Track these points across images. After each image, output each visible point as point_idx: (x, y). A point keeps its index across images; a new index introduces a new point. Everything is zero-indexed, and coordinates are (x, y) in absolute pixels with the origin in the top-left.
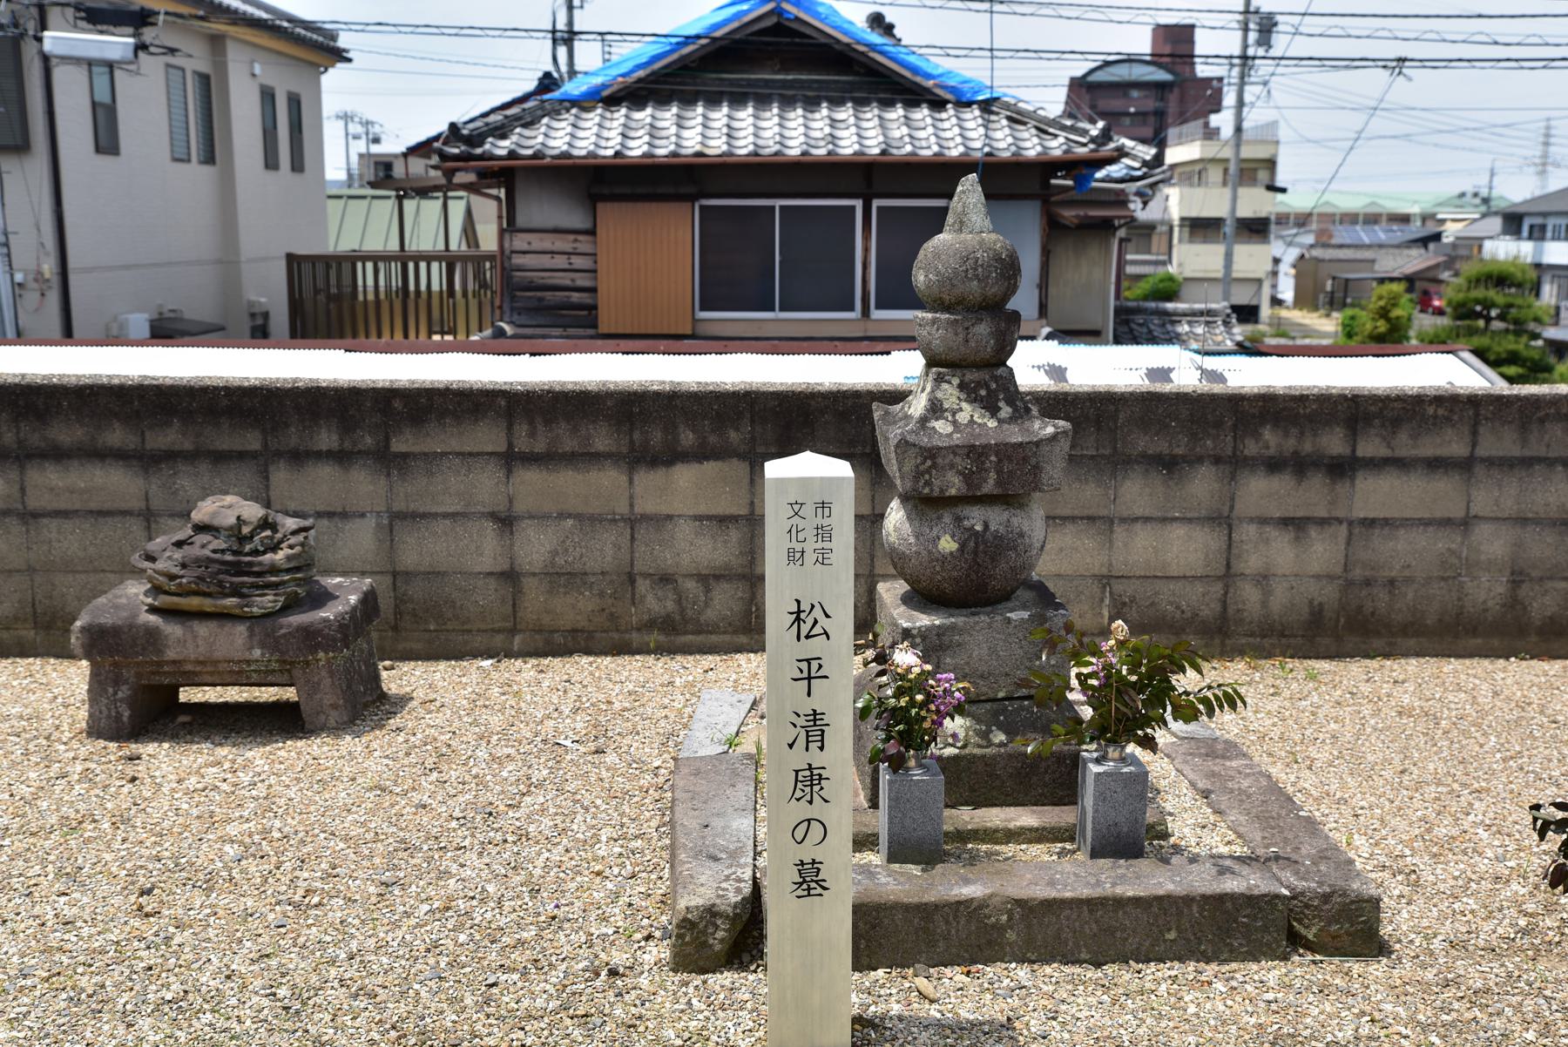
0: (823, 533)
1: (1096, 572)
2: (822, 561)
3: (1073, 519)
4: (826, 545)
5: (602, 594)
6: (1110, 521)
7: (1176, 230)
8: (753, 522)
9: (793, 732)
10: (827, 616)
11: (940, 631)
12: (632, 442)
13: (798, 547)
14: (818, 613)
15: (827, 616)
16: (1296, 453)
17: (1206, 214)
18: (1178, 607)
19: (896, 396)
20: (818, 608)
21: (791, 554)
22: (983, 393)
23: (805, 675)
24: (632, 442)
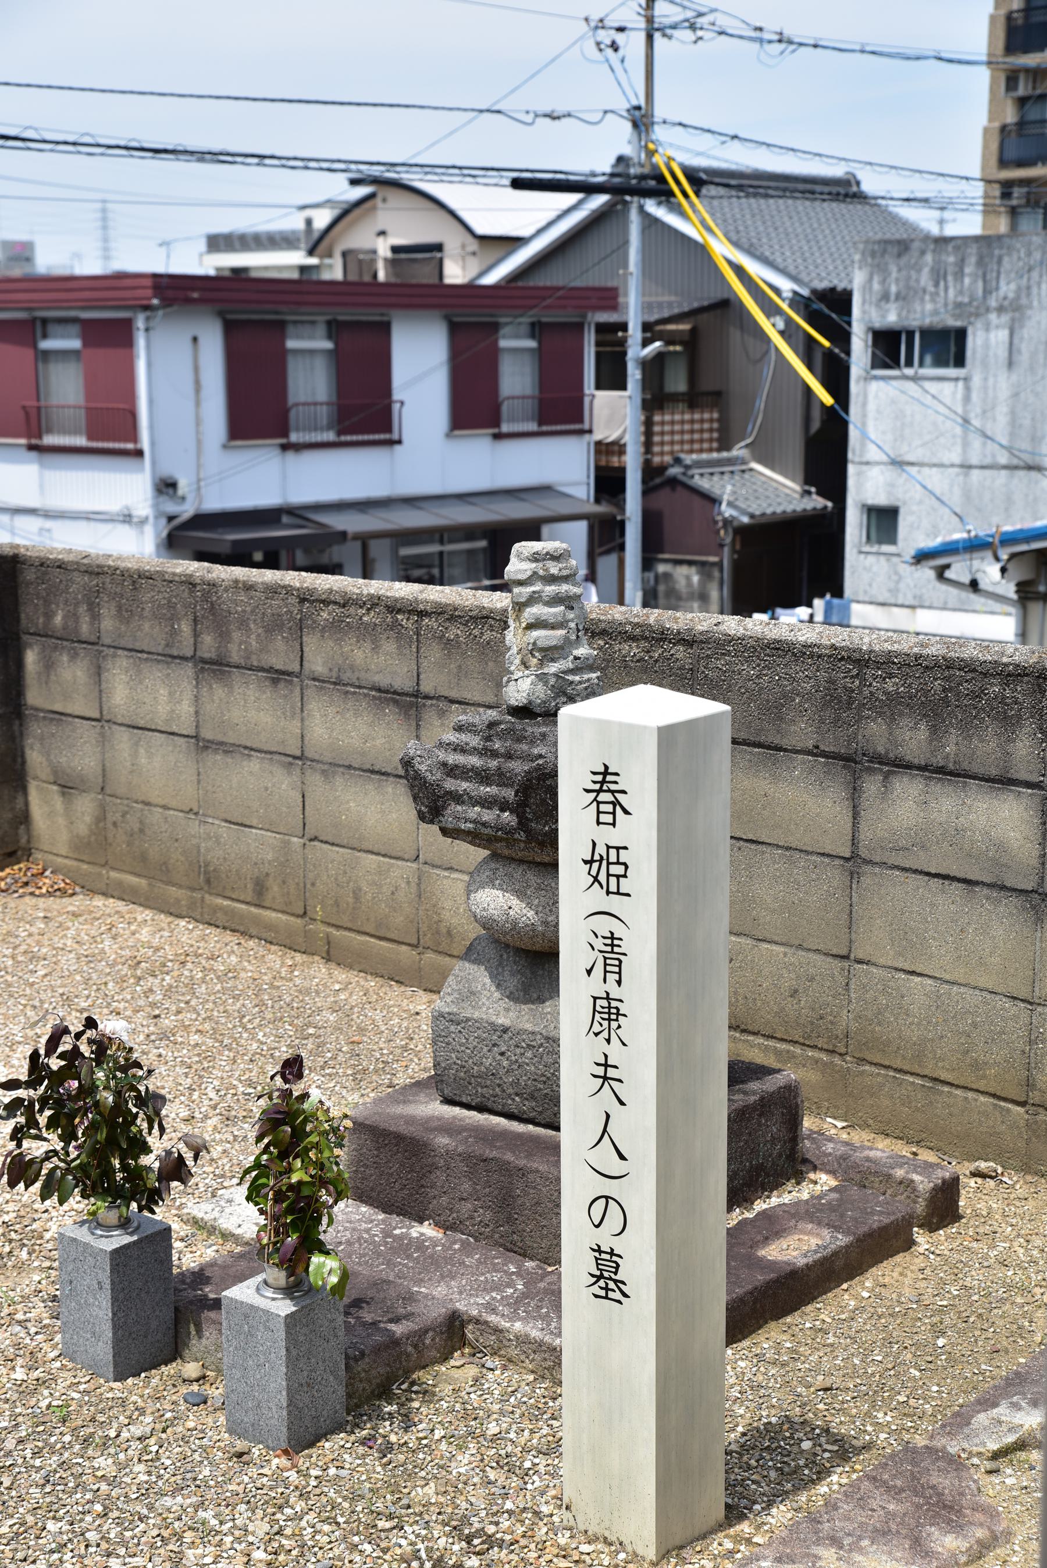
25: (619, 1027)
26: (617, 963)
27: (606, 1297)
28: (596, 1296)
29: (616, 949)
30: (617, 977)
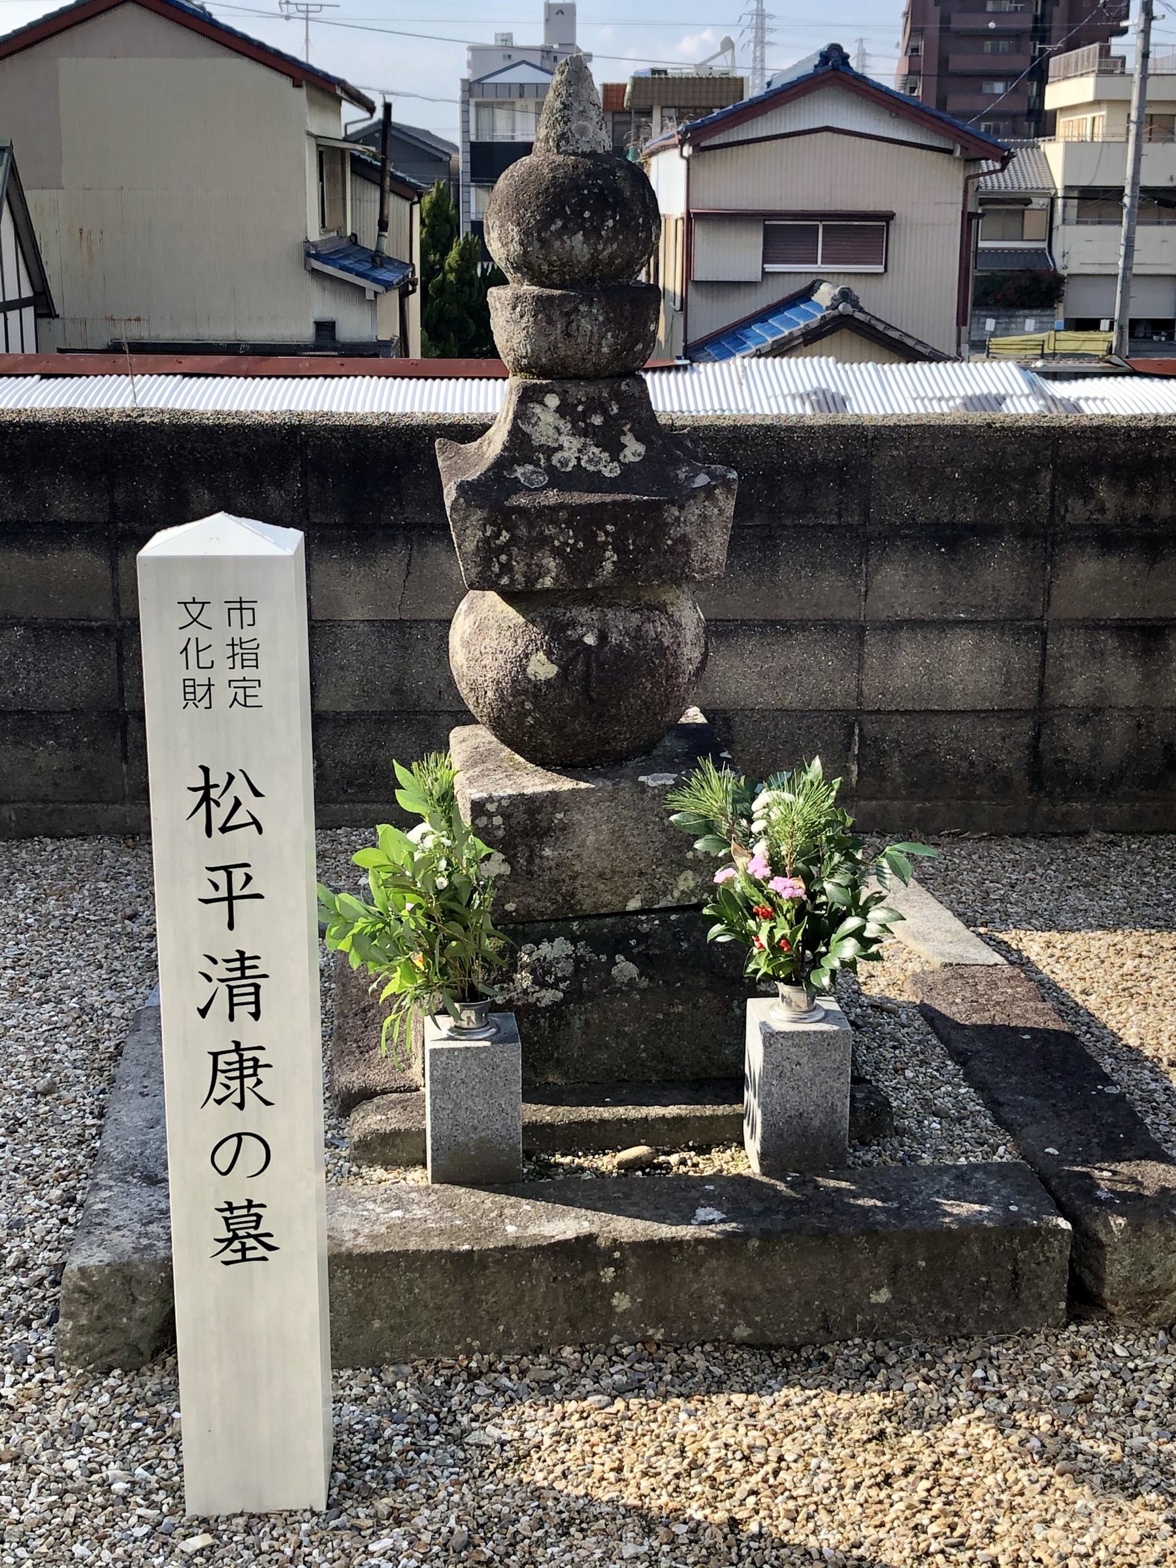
0: (243, 653)
1: (838, 704)
2: (244, 697)
3: (803, 625)
4: (250, 673)
5: (74, 744)
6: (859, 631)
7: (1060, 202)
8: (120, 636)
9: (207, 989)
10: (257, 794)
11: (531, 804)
12: (113, 505)
13: (201, 677)
14: (239, 788)
15: (257, 794)
16: (1146, 519)
17: (1100, 182)
18: (964, 757)
19: (468, 431)
20: (239, 779)
21: (189, 686)
22: (597, 420)
23: (223, 892)
24: (113, 505)
25: (259, 1082)
26: (252, 989)
27: (244, 1259)
28: (227, 1263)
29: (248, 973)
30: (252, 1008)
